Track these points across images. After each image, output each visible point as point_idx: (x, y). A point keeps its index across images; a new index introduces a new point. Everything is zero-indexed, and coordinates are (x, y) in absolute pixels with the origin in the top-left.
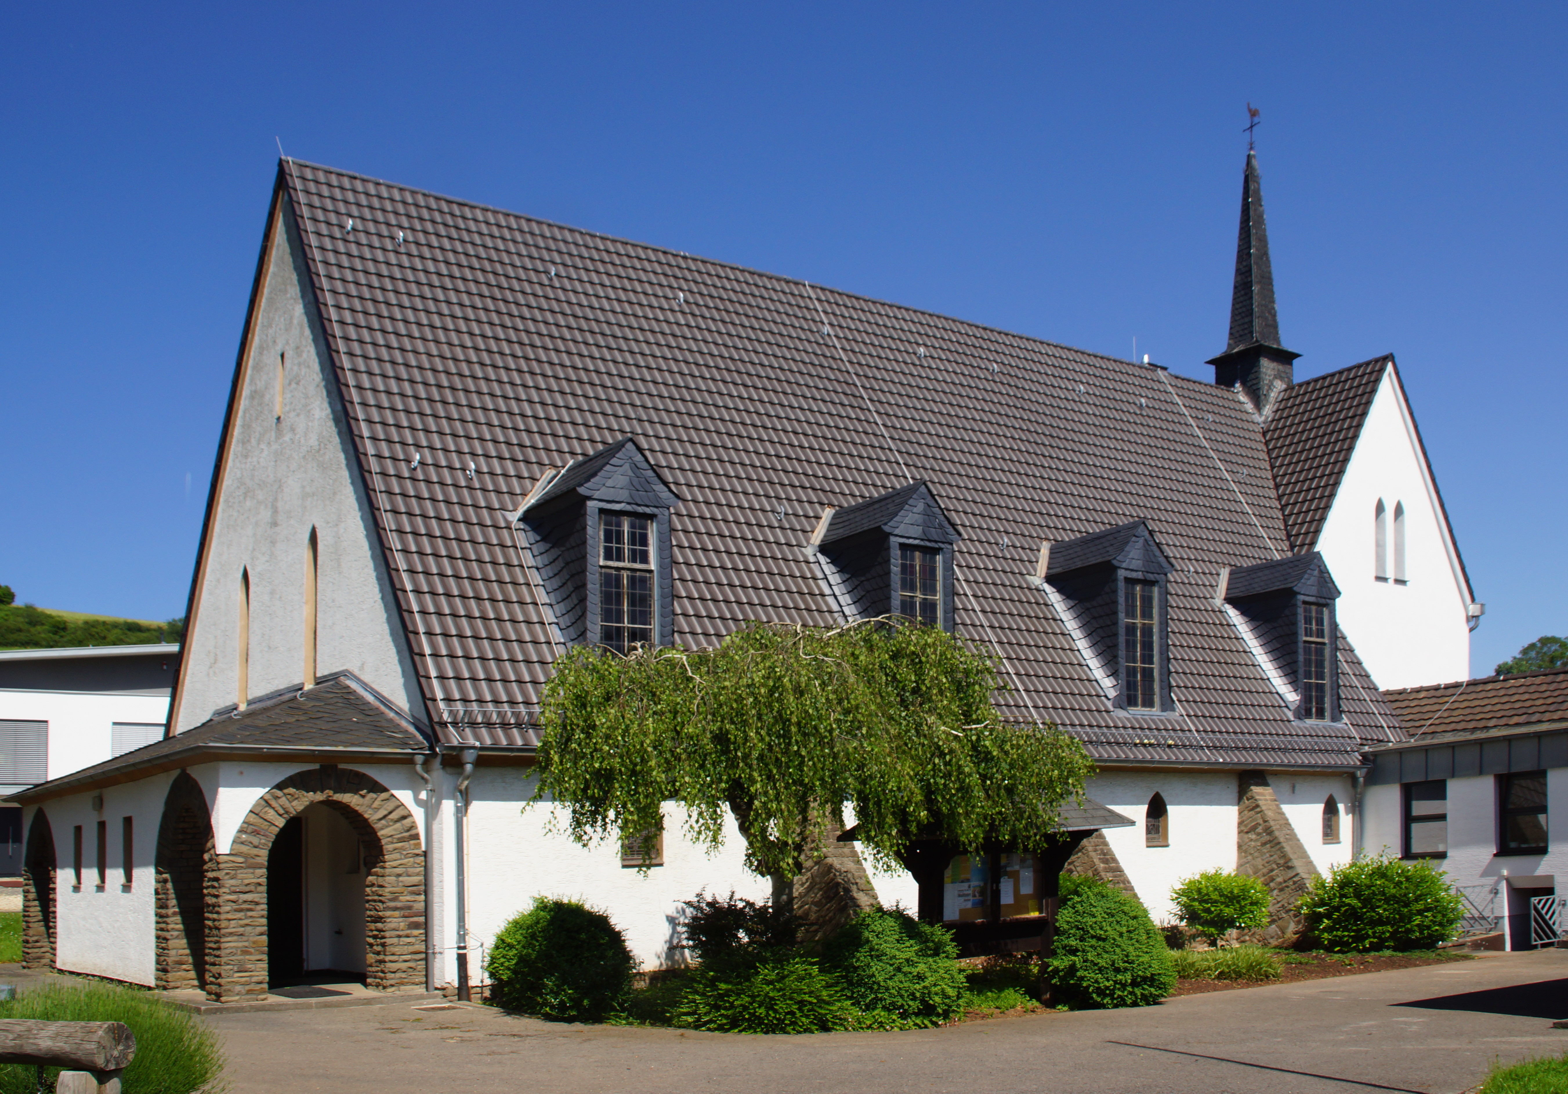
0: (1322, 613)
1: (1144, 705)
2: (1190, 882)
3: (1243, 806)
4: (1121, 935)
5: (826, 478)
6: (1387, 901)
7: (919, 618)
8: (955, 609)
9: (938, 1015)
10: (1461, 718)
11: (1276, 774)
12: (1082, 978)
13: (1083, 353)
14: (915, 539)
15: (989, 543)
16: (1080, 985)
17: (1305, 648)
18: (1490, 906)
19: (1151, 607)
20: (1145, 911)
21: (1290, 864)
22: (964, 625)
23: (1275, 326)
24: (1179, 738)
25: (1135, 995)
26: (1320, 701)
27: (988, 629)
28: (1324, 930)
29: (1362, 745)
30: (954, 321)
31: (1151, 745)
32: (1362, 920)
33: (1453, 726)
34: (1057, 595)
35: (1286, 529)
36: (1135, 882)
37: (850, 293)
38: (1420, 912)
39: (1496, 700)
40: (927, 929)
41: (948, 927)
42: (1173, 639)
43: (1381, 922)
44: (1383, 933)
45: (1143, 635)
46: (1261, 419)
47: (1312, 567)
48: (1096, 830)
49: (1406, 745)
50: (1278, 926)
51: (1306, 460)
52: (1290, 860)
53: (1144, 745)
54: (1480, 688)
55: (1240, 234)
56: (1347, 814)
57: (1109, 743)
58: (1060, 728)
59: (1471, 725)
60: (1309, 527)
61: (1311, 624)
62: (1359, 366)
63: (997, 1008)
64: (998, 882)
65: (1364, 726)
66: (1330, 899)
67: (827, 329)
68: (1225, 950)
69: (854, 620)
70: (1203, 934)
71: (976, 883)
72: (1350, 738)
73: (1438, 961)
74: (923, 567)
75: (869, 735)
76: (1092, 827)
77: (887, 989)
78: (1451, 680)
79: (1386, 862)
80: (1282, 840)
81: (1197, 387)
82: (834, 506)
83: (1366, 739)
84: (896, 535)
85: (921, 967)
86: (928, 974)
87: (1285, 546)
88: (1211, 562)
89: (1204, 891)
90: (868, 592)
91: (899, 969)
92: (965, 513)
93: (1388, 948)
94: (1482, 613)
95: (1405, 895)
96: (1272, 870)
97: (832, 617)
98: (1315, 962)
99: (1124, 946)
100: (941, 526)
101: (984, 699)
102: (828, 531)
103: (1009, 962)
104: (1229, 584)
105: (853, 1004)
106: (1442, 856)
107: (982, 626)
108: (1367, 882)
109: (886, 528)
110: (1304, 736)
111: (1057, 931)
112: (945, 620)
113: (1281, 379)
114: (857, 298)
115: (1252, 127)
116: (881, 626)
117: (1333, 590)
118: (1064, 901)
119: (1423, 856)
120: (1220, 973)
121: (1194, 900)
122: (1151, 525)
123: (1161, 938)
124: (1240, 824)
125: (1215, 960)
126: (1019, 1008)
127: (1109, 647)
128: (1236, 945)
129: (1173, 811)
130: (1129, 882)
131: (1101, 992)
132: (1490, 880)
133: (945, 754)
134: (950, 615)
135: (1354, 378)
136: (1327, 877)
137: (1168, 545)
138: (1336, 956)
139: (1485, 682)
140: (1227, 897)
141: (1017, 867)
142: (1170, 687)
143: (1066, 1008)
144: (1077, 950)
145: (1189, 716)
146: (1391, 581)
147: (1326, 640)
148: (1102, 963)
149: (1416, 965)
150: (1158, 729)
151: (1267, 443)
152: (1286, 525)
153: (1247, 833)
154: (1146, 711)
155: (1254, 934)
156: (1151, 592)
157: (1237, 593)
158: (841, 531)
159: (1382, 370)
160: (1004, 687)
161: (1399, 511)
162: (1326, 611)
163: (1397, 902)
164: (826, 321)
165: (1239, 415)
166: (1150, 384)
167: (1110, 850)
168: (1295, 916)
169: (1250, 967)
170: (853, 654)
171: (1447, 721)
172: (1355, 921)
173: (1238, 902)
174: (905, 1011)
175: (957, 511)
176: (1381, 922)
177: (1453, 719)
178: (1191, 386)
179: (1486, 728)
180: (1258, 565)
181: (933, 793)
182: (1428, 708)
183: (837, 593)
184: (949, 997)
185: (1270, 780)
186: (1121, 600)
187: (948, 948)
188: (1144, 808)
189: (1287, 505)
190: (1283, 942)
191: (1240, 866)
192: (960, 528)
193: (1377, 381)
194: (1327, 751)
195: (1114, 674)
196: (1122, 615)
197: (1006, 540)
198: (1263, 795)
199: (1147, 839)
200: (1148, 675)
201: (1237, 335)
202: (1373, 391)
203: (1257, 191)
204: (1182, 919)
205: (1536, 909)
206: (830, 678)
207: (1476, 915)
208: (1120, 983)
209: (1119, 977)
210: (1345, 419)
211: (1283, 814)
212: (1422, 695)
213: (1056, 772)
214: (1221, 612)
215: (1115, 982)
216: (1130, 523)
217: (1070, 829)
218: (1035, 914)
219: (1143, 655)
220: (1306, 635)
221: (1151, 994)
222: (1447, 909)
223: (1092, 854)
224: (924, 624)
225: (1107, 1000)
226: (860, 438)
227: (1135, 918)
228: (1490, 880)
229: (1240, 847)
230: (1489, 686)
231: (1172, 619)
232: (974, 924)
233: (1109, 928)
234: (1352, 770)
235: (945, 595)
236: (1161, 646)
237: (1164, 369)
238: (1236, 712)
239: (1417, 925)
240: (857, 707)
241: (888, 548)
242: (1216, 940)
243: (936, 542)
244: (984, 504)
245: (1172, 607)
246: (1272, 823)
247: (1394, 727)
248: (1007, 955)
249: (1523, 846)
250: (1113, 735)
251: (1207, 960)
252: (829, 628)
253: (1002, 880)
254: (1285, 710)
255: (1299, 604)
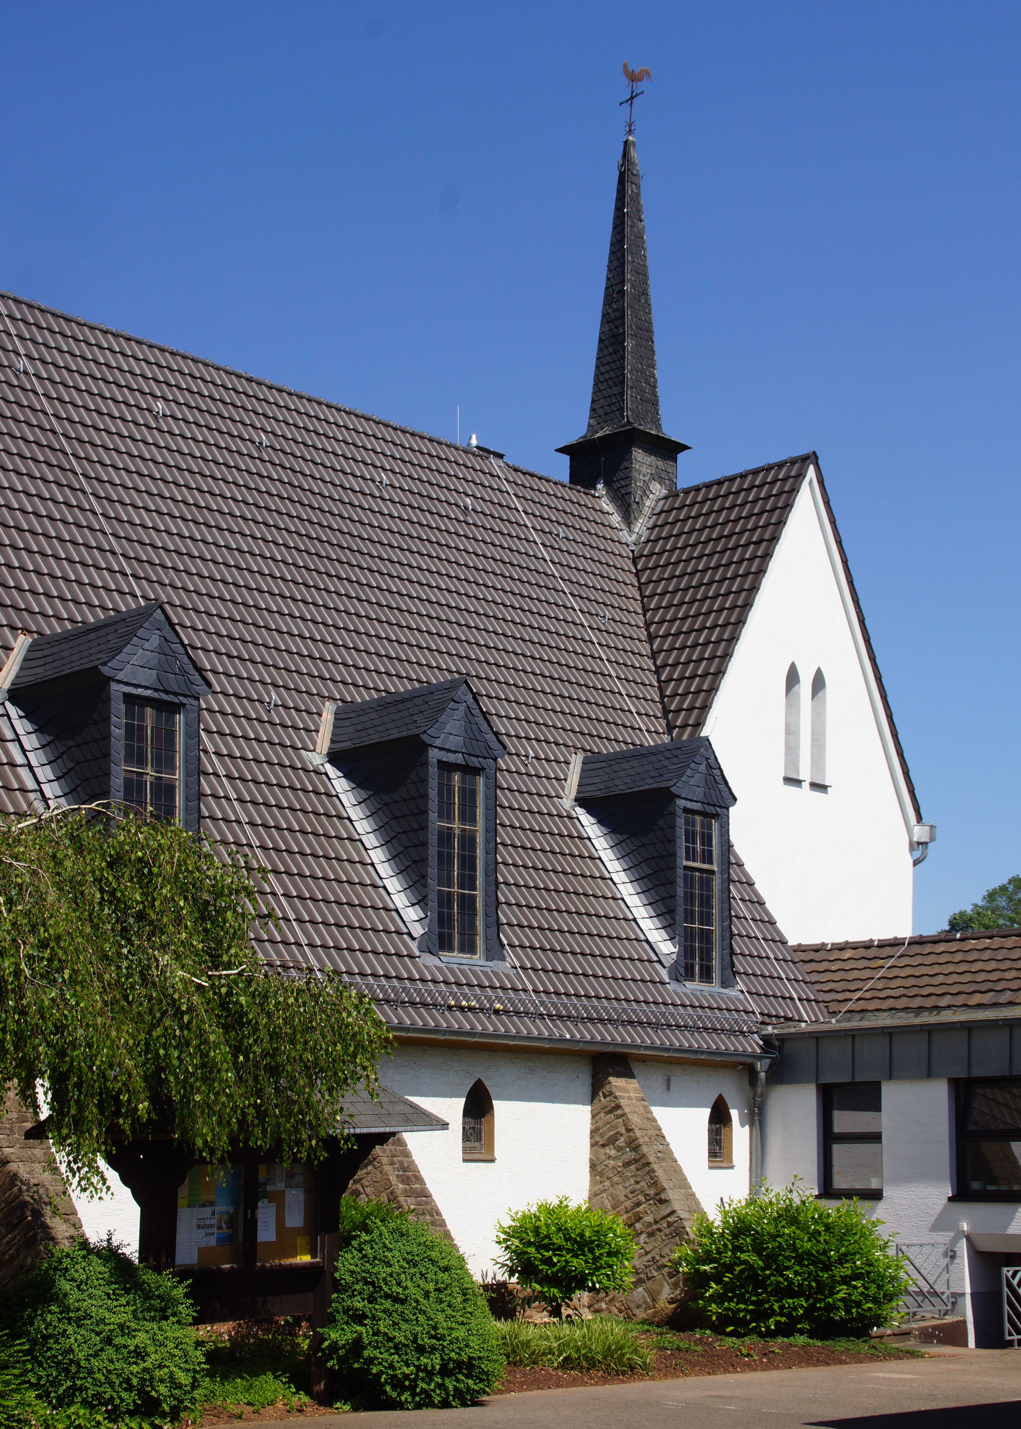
0: (710, 827)
1: (462, 950)
2: (524, 1217)
3: (598, 1105)
4: (427, 1295)
5: (19, 589)
6: (799, 1259)
7: (150, 808)
8: (201, 795)
9: (163, 1415)
10: (902, 991)
11: (643, 1060)
12: (371, 1361)
13: (386, 426)
14: (146, 688)
15: (251, 700)
16: (368, 1371)
17: (685, 875)
18: (945, 1276)
19: (474, 807)
20: (461, 1259)
21: (663, 1196)
22: (213, 818)
23: (654, 402)
24: (510, 1000)
25: (446, 1389)
26: (706, 955)
27: (247, 827)
28: (712, 1299)
29: (763, 1023)
30: (206, 365)
31: (471, 1009)
32: (765, 1288)
33: (890, 1003)
34: (343, 780)
35: (662, 702)
36: (447, 1215)
37: (57, 311)
38: (846, 1280)
39: (950, 968)
40: (149, 1277)
41: (183, 1274)
42: (504, 854)
43: (790, 1291)
44: (795, 1309)
45: (462, 847)
46: (631, 539)
47: (697, 759)
48: (394, 1134)
49: (825, 1027)
50: (646, 1290)
51: (691, 602)
52: (664, 1189)
53: (462, 1009)
54: (928, 948)
55: (610, 261)
56: (743, 1125)
57: (413, 1004)
58: (346, 978)
59: (916, 1003)
60: (694, 701)
61: (694, 842)
62: (768, 469)
63: (249, 1404)
64: (254, 1208)
65: (767, 996)
66: (719, 1253)
67: (22, 363)
68: (571, 1322)
69: (59, 805)
70: (541, 1297)
71: (222, 1207)
72: (747, 1012)
73: (873, 1358)
74: (156, 730)
75: (73, 981)
76: (388, 1130)
77: (90, 1372)
78: (887, 935)
79: (797, 1201)
80: (652, 1159)
81: (544, 486)
82: (31, 632)
83: (769, 1016)
84: (120, 682)
85: (141, 1338)
86: (151, 1349)
87: (660, 725)
88: (557, 744)
89: (544, 1231)
90: (78, 763)
91: (108, 1341)
92: (218, 653)
93: (801, 1332)
94: (932, 839)
95: (825, 1252)
96: (638, 1204)
97: (26, 800)
98: (699, 1348)
99: (430, 1312)
100: (184, 672)
101: (238, 935)
102: (22, 669)
103: (267, 1331)
104: (581, 778)
105: (38, 1397)
106: (876, 1195)
107: (238, 822)
108: (771, 1229)
109: (106, 670)
110: (683, 1006)
111: (337, 1286)
112: (187, 810)
113: (661, 481)
114: (68, 320)
115: (632, 98)
116: (95, 816)
117: (726, 795)
118: (347, 1241)
119: (848, 1194)
120: (566, 1359)
121: (529, 1244)
122: (477, 685)
123: (482, 1302)
124: (593, 1132)
125: (557, 1338)
126: (280, 1405)
127: (415, 862)
128: (588, 1316)
129: (499, 1106)
130: (438, 1213)
131: (397, 1383)
132: (944, 1237)
133: (183, 1013)
134: (194, 803)
135: (761, 486)
136: (715, 1217)
137: (499, 716)
138: (730, 1342)
139: (935, 941)
140: (575, 1241)
141: (281, 1186)
142: (499, 924)
143: (347, 1407)
144: (364, 1316)
145: (523, 968)
146: (806, 785)
147: (715, 868)
148: (399, 1336)
149: (841, 1362)
150: (481, 986)
151: (638, 575)
152: (662, 696)
153: (603, 1146)
154: (464, 958)
155: (613, 1299)
156: (474, 784)
157: (592, 792)
158: (40, 670)
159: (800, 476)
160: (269, 916)
161: (819, 683)
162: (715, 825)
163: (814, 1263)
164: (22, 351)
165: (601, 531)
166: (479, 478)
167: (413, 1162)
168: (671, 1275)
169: (608, 1352)
170: (54, 857)
171: (882, 995)
172: (755, 1289)
173: (591, 1250)
174: (116, 1407)
175: (205, 650)
176: (790, 1291)
177: (889, 992)
178: (535, 483)
179: (936, 1008)
180: (622, 752)
181: (162, 1069)
182: (855, 974)
183: (34, 762)
184: (180, 1386)
185: (636, 1070)
186: (433, 793)
187: (181, 1308)
188: (460, 1103)
189: (665, 666)
190: (654, 1315)
191: (593, 1195)
192: (210, 676)
193: (794, 491)
194: (715, 1030)
195: (421, 902)
196: (433, 816)
197: (274, 696)
198: (625, 1090)
199: (465, 1150)
200: (468, 904)
201: (601, 412)
202: (788, 506)
203: (636, 198)
204: (512, 1272)
205: (1010, 1285)
206: (20, 893)
207: (926, 1288)
208: (425, 1370)
209: (424, 1360)
210: (746, 546)
211: (654, 1120)
212: (848, 954)
213: (339, 1047)
214: (570, 818)
215: (418, 1368)
216: (447, 681)
217: (358, 1131)
218: (306, 1258)
219: (461, 877)
220: (688, 859)
221: (468, 1388)
222: (883, 1277)
223: (387, 1168)
224: (157, 817)
225: (406, 1396)
226: (70, 533)
227: (446, 1269)
228: (944, 1237)
229: (593, 1166)
230: (941, 947)
231: (502, 825)
232: (220, 1270)
233: (409, 1284)
234: (749, 1060)
235: (188, 774)
236: (487, 864)
237: (500, 456)
238: (590, 966)
239: (843, 1300)
240: (58, 938)
241: (108, 700)
242: (559, 1306)
243: (176, 694)
244: (243, 641)
245: (503, 807)
246: (638, 1133)
247: (808, 1000)
248: (267, 1321)
249: (990, 1188)
250: (418, 991)
251: (547, 1338)
252: (21, 816)
253: (260, 1204)
254: (658, 966)
255: (679, 812)
